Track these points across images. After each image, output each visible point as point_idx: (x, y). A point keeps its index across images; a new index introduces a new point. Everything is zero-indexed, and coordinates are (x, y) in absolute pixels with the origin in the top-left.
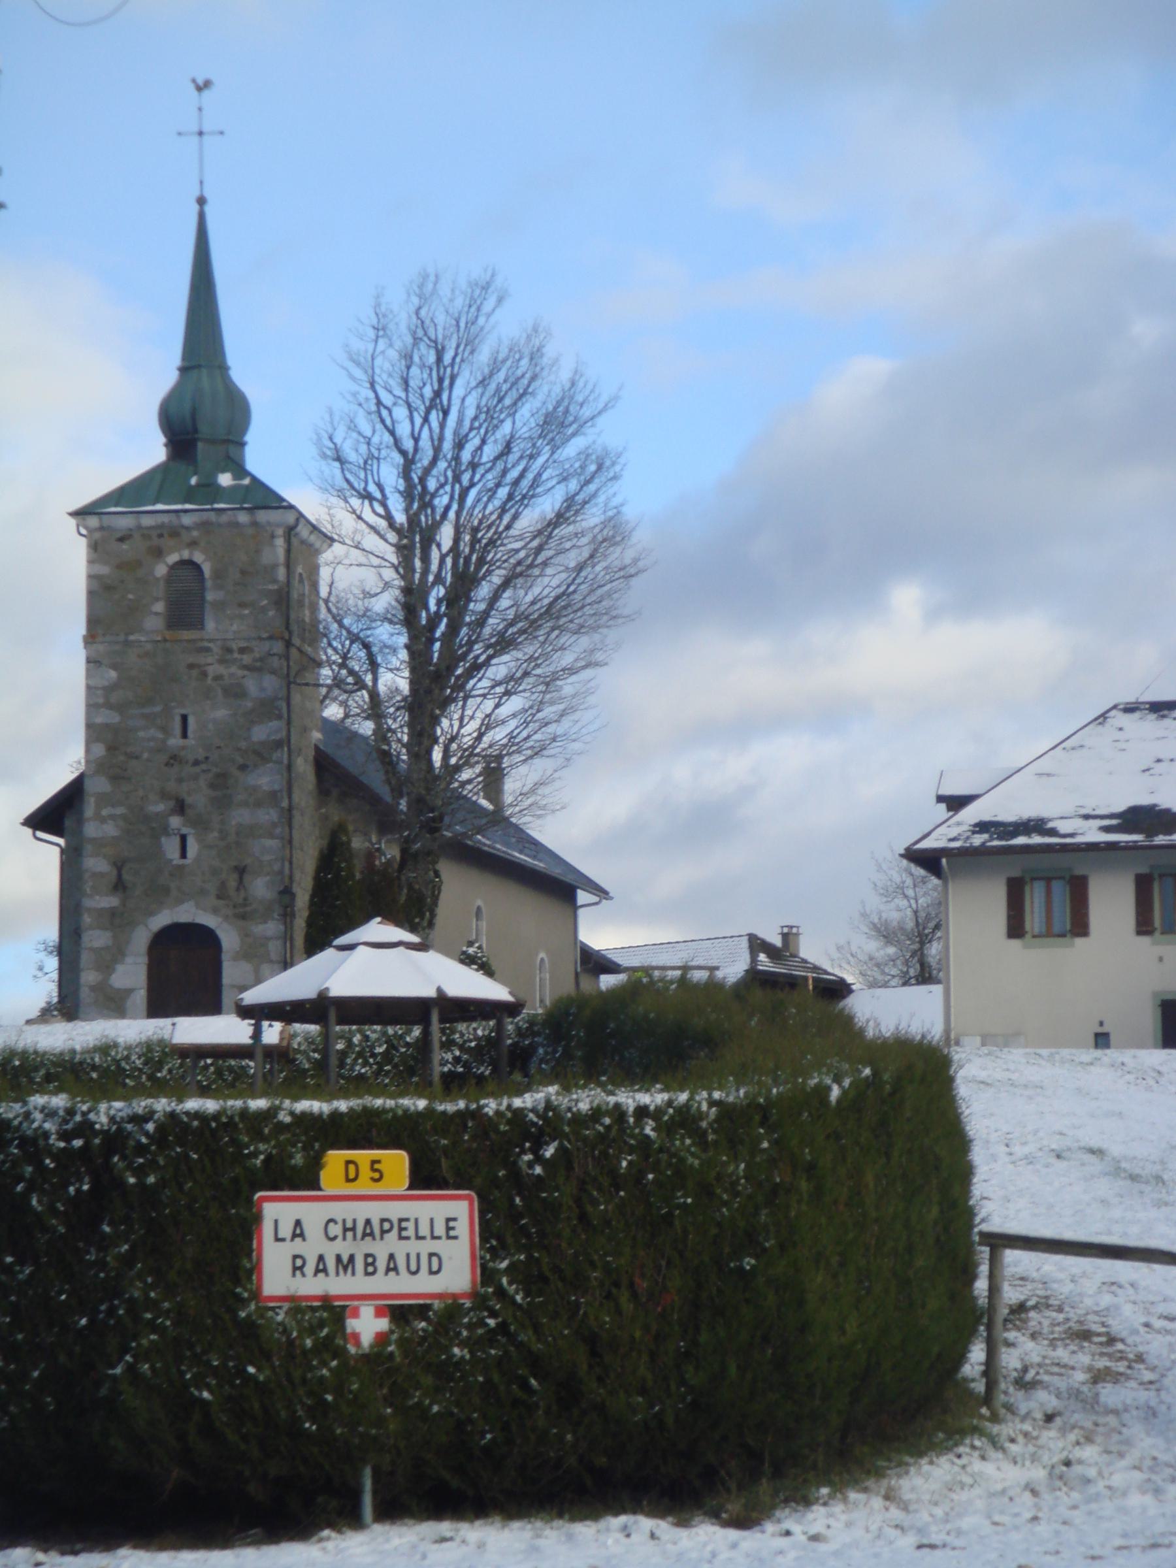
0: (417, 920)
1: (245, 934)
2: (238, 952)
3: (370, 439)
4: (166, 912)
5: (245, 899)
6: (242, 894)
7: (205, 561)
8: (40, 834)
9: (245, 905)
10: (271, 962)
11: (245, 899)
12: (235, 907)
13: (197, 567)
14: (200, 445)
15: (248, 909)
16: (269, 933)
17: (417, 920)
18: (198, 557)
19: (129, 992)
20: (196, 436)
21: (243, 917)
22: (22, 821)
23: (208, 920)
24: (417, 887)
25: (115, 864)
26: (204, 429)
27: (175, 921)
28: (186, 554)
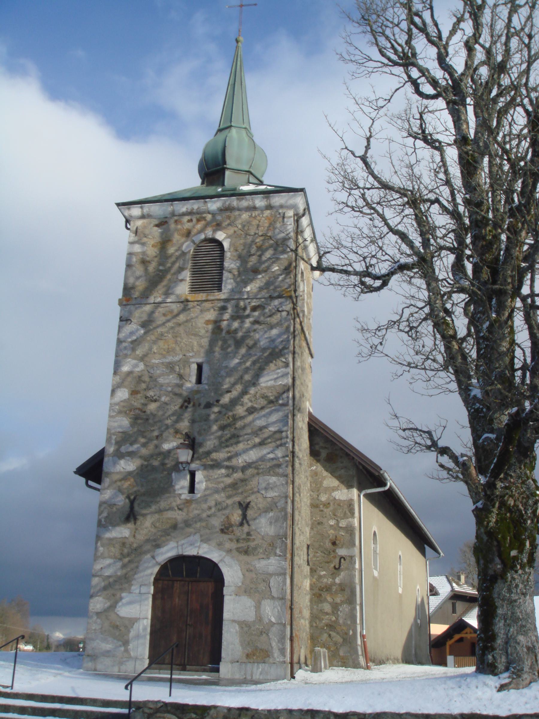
0: (514, 553)
1: (248, 570)
2: (240, 587)
3: (347, 203)
4: (172, 544)
5: (248, 534)
6: (246, 528)
7: (225, 238)
8: (91, 483)
9: (248, 540)
10: (273, 598)
11: (248, 534)
12: (238, 541)
13: (220, 244)
14: (227, 173)
15: (252, 544)
16: (271, 569)
17: (514, 553)
18: (220, 236)
19: (133, 621)
20: (225, 166)
21: (246, 552)
22: (75, 470)
23: (214, 556)
24: (511, 502)
25: (128, 497)
26: (231, 163)
27: (180, 553)
28: (209, 233)
